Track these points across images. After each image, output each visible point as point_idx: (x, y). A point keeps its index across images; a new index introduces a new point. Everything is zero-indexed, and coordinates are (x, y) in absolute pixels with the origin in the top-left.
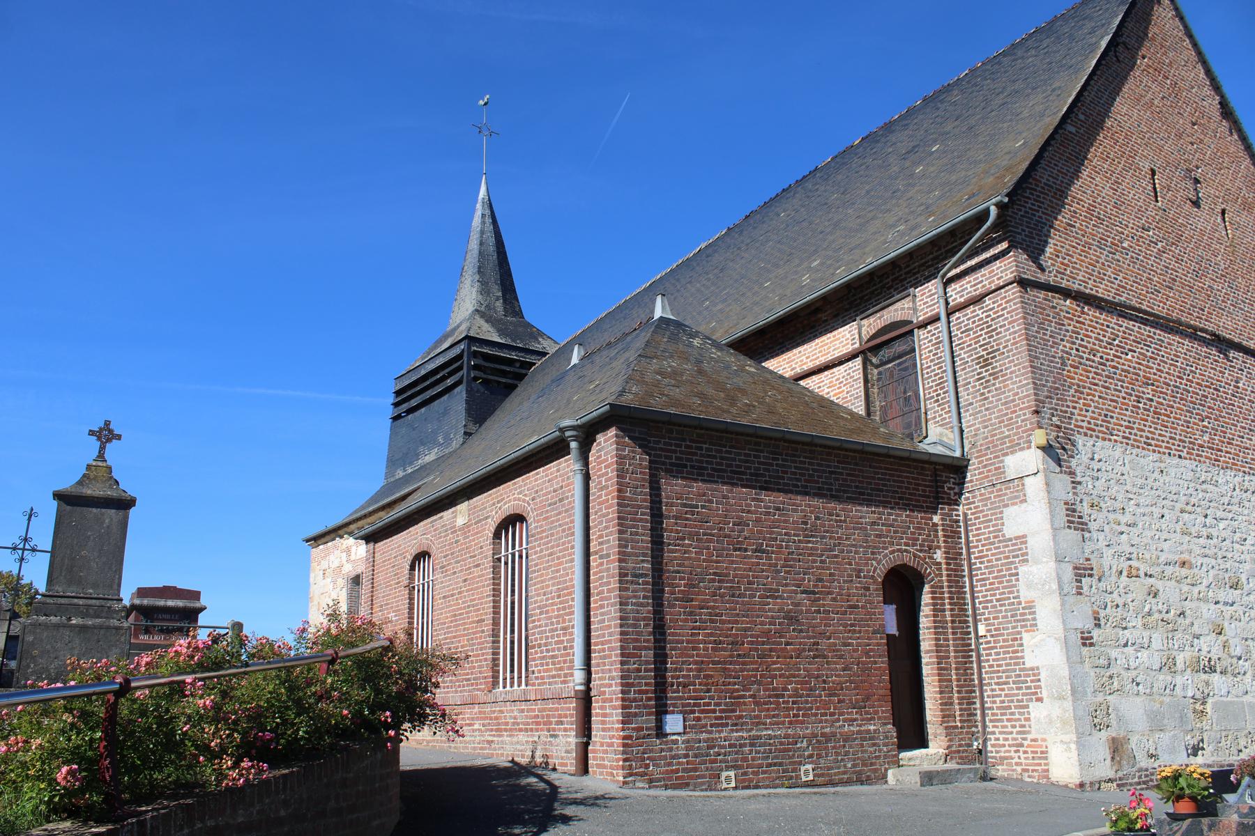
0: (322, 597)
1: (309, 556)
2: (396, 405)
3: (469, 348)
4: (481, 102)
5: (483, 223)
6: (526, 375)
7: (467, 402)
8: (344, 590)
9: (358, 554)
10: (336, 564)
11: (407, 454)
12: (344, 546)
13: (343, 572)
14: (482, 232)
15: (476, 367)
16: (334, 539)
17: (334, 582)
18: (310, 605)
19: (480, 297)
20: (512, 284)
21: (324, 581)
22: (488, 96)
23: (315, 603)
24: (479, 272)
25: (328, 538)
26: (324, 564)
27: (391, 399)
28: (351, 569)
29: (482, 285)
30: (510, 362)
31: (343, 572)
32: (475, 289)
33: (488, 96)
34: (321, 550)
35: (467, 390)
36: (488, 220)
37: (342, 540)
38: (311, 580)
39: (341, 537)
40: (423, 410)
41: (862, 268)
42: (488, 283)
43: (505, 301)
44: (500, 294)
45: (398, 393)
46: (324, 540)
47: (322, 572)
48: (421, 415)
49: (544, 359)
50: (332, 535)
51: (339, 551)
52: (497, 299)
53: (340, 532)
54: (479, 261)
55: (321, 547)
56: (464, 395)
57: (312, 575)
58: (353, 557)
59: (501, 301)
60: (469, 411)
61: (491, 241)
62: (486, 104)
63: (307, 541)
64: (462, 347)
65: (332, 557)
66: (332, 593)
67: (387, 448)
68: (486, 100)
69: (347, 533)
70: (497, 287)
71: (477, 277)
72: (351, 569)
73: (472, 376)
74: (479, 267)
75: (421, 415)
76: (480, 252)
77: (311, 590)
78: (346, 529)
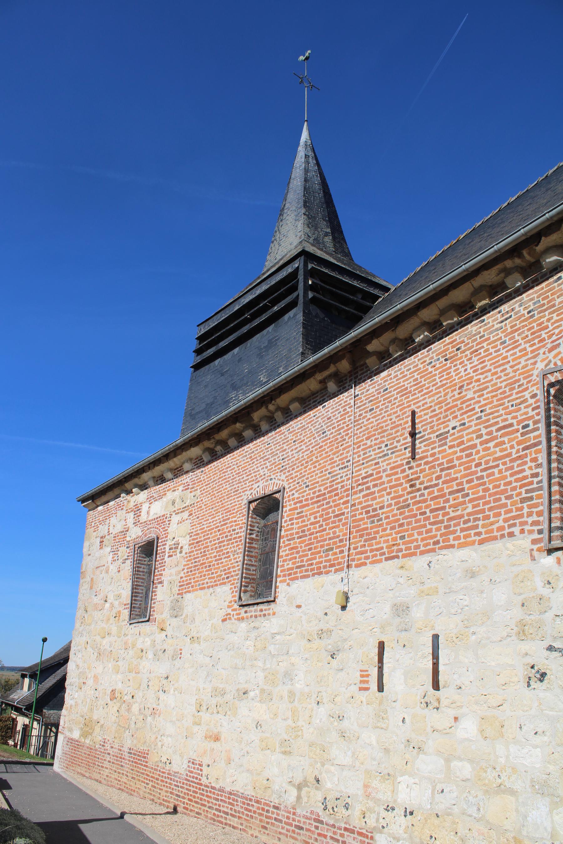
0: (98, 572)
1: (85, 519)
2: (198, 352)
3: (306, 265)
4: (302, 58)
5: (307, 162)
6: (372, 307)
7: (305, 326)
8: (128, 562)
9: (151, 513)
10: (119, 528)
11: (212, 403)
12: (132, 504)
13: (128, 539)
14: (306, 171)
15: (313, 288)
16: (118, 496)
17: (115, 552)
18: (82, 581)
19: (307, 230)
20: (339, 225)
21: (102, 551)
22: (309, 52)
23: (88, 579)
24: (305, 206)
25: (110, 495)
26: (103, 530)
27: (195, 345)
28: (140, 534)
29: (309, 218)
30: (355, 290)
31: (128, 539)
32: (301, 222)
33: (309, 52)
34: (101, 512)
35: (304, 312)
36: (312, 162)
37: (129, 497)
38: (85, 550)
39: (129, 492)
40: (236, 350)
41: (96, 798)
42: (315, 218)
43: (334, 239)
44: (329, 230)
45: (201, 339)
46: (104, 498)
47: (98, 540)
48: (234, 356)
49: (387, 294)
50: (116, 491)
51: (124, 512)
52: (326, 234)
53: (128, 485)
54: (304, 196)
55: (100, 508)
56: (300, 317)
57: (86, 544)
58: (144, 517)
59: (331, 237)
60: (306, 337)
61: (317, 180)
62: (307, 58)
63: (83, 501)
64: (297, 266)
65: (113, 520)
66: (111, 567)
67: (328, 182)
68: (307, 54)
69: (136, 486)
70: (325, 223)
71: (303, 211)
72: (140, 534)
73: (310, 297)
74: (305, 202)
75: (234, 356)
76: (305, 188)
77: (84, 562)
78: (136, 481)
